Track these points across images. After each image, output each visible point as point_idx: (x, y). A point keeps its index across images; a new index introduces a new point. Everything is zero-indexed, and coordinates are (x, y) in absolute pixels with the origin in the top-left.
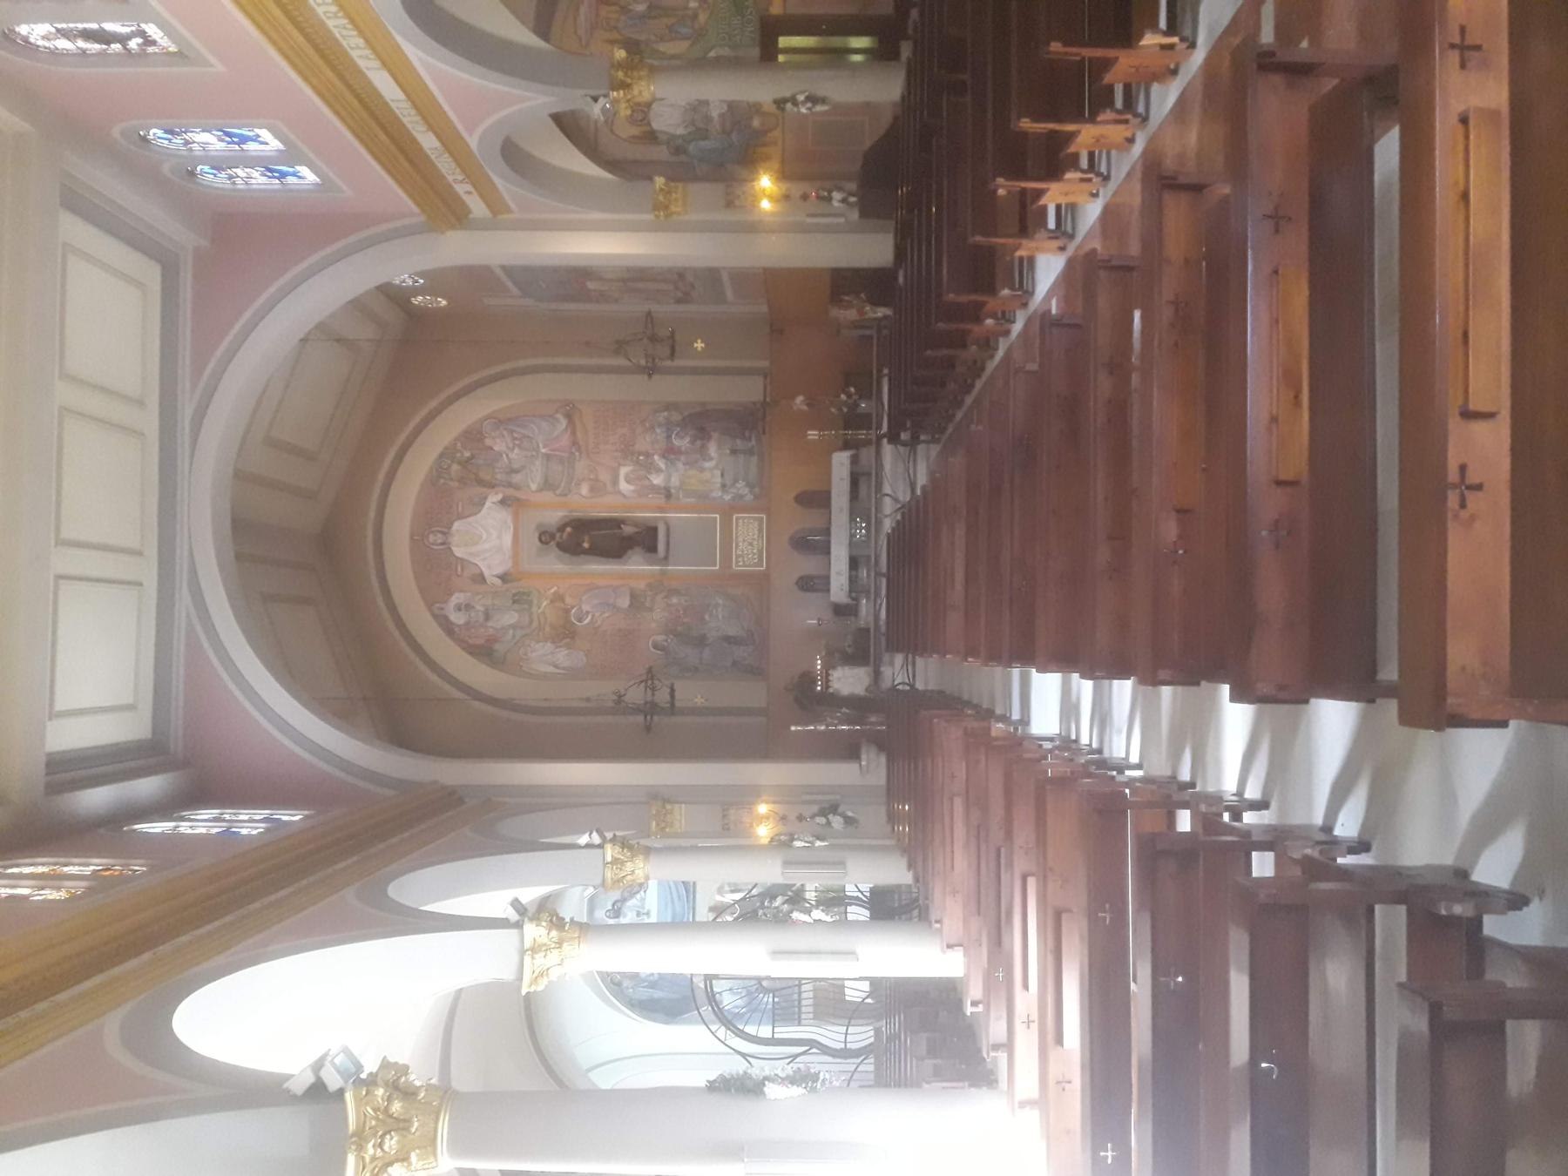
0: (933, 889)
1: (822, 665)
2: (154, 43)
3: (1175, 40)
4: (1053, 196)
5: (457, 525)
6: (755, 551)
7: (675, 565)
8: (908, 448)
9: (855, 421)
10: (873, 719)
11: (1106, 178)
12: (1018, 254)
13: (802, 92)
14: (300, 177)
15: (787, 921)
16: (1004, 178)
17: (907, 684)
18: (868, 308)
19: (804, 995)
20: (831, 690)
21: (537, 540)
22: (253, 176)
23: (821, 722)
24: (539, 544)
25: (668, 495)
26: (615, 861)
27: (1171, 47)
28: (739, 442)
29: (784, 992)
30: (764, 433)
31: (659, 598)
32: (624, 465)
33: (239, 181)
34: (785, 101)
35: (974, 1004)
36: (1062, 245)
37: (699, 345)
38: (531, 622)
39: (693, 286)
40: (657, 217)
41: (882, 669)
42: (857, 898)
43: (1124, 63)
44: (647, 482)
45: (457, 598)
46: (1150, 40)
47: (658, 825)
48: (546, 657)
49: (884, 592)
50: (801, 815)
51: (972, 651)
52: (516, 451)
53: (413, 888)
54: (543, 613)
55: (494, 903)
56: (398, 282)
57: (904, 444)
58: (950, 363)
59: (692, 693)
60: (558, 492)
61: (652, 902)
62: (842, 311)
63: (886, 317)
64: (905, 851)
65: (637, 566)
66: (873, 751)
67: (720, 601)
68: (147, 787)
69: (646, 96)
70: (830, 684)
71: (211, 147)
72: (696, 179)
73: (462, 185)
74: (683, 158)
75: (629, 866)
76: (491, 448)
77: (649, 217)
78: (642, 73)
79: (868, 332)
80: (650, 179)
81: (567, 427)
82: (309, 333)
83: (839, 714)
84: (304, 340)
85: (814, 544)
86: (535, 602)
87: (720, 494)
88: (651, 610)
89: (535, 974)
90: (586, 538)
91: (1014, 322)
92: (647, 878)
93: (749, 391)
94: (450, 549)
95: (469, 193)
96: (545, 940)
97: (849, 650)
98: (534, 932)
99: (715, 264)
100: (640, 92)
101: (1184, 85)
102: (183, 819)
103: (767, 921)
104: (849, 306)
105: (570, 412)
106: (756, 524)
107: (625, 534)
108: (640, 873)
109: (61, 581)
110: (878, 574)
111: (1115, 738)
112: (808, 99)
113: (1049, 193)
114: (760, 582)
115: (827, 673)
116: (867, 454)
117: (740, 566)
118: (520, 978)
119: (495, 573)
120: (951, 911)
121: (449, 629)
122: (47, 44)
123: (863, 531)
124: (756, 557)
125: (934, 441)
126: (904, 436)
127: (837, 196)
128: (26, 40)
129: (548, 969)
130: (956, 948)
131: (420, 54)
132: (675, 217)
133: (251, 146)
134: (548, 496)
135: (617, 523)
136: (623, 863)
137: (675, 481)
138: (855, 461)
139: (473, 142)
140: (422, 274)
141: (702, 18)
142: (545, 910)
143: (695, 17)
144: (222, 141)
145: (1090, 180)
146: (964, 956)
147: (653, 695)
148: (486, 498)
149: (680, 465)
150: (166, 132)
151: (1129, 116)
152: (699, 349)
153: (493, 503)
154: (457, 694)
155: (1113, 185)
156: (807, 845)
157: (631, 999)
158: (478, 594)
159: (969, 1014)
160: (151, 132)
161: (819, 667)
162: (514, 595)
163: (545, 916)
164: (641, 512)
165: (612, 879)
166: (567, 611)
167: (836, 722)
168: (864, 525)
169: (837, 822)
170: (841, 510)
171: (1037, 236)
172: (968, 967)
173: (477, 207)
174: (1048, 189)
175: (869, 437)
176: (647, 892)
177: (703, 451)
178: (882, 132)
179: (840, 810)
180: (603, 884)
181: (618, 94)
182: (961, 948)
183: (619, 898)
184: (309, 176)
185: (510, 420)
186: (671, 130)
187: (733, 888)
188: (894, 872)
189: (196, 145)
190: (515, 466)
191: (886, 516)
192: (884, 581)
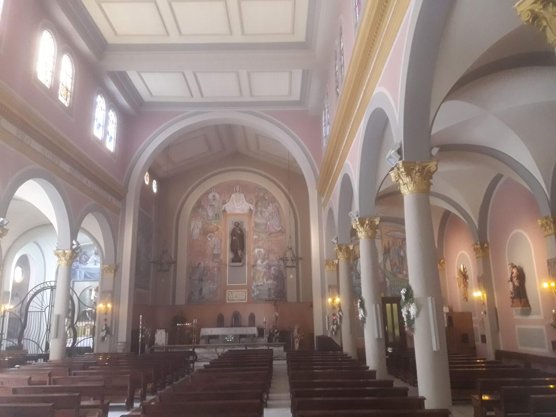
5: (242, 195)
13: (342, 314)
28: (273, 291)
31: (217, 264)
45: (217, 196)
47: (107, 267)
48: (197, 226)
52: (268, 214)
54: (212, 224)
60: (254, 228)
65: (229, 255)
67: (215, 286)
83: (148, 333)
87: (254, 285)
88: (213, 261)
90: (236, 238)
94: (234, 193)
106: (244, 298)
107: (238, 251)
134: (253, 224)
137: (259, 268)
143: (400, 273)
148: (251, 204)
149: (264, 270)
152: (291, 278)
153: (250, 207)
158: (219, 203)
161: (186, 324)
162: (218, 214)
166: (213, 232)
169: (103, 334)
179: (108, 335)
185: (279, 211)
190: (263, 214)
191: (216, 350)
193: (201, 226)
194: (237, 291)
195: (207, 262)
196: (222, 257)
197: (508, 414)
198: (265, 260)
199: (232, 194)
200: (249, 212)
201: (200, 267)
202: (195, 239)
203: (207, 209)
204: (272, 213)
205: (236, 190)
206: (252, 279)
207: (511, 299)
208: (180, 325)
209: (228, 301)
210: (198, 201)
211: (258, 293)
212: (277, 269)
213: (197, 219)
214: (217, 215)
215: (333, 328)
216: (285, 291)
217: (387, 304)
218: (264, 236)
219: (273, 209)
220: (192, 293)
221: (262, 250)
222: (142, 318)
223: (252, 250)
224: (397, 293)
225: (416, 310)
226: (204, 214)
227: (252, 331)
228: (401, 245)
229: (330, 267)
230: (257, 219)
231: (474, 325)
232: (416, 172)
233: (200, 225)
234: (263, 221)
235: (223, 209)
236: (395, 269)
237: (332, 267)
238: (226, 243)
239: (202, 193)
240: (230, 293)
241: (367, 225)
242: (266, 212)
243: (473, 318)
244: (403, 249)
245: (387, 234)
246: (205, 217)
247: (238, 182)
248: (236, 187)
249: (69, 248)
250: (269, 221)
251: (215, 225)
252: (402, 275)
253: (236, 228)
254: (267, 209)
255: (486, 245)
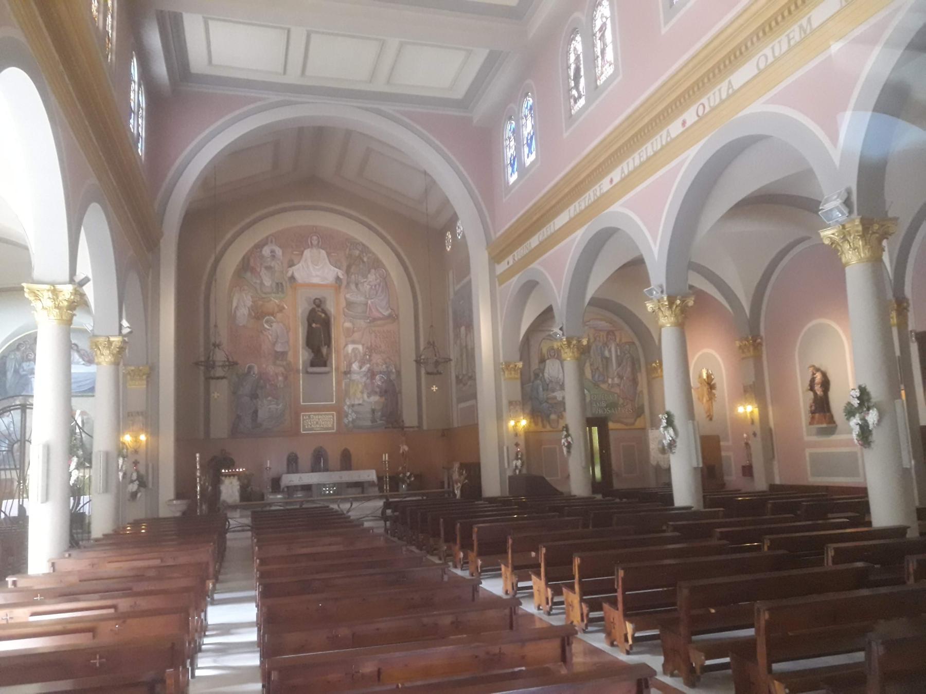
0: (95, 551)
1: (239, 472)
2: (575, 102)
3: (630, 642)
4: (537, 583)
5: (323, 252)
6: (313, 426)
8: (381, 516)
9: (395, 482)
10: (204, 507)
11: (549, 614)
13: (572, 440)
14: (511, 174)
15: (71, 454)
17: (229, 527)
18: (459, 484)
19: (8, 472)
20: (223, 478)
22: (511, 150)
24: (314, 298)
26: (110, 343)
27: (626, 640)
29: (11, 459)
30: (386, 428)
31: (282, 369)
32: (363, 348)
33: (508, 142)
34: (567, 431)
36: (508, 592)
37: (434, 388)
38: (265, 293)
39: (465, 385)
41: (238, 511)
42: (79, 503)
43: (615, 615)
44: (353, 360)
45: (279, 252)
46: (629, 627)
47: (132, 370)
48: (243, 304)
49: (288, 507)
51: (263, 562)
52: (368, 287)
53: (96, 217)
54: (271, 300)
55: (85, 268)
56: (458, 224)
57: (383, 513)
58: (436, 534)
59: (220, 393)
61: (79, 369)
62: (457, 469)
63: (455, 495)
65: (302, 356)
66: (184, 508)
67: (281, 406)
68: (160, 68)
69: (564, 356)
71: (524, 129)
72: (523, 384)
75: (106, 352)
77: (501, 360)
78: (576, 353)
79: (446, 486)
80: (521, 360)
82: (430, 176)
83: (207, 484)
84: (425, 173)
85: (319, 462)
87: (348, 403)
89: (37, 292)
90: (318, 326)
91: (462, 570)
92: (99, 364)
93: (409, 417)
94: (309, 248)
95: (508, 263)
96: (60, 298)
98: (67, 291)
99: (479, 396)
100: (566, 353)
101: (607, 651)
102: (139, 85)
104: (461, 474)
105: (393, 318)
106: (330, 426)
108: (101, 359)
109: (286, 31)
110: (302, 503)
111: (209, 659)
112: (569, 443)
114: (294, 432)
116: (375, 491)
117: (303, 417)
119: (294, 271)
120: (77, 564)
123: (328, 492)
124: (309, 427)
125: (386, 530)
126: (389, 512)
127: (519, 463)
128: (573, 39)
129: (40, 300)
130: (52, 568)
131: (580, 237)
132: (502, 373)
133: (526, 150)
134: (343, 304)
135: (328, 343)
136: (109, 348)
137: (355, 377)
138: (371, 484)
140: (464, 237)
141: (604, 386)
142: (78, 303)
143: (604, 382)
144: (528, 135)
145: (547, 603)
146: (43, 574)
148: (339, 269)
149: (364, 379)
150: (531, 107)
151: (585, 621)
153: (337, 273)
154: (219, 248)
155: (546, 618)
156: (120, 467)
157: (6, 357)
158: (282, 263)
159: (7, 579)
161: (237, 470)
162: (281, 284)
163: (78, 298)
164: (335, 357)
165: (98, 341)
166: (272, 314)
168: (331, 492)
169: (134, 487)
170: (341, 477)
171: (514, 577)
172: (36, 577)
173: (501, 268)
174: (541, 580)
175: (385, 491)
176: (83, 366)
178: (554, 485)
179: (142, 489)
180: (95, 336)
181: (565, 341)
182: (52, 571)
183: (80, 348)
184: (513, 178)
185: (386, 283)
186: (546, 371)
187: (85, 421)
188: (100, 526)
189: (525, 121)
190: (360, 286)
192: (298, 507)
193: (251, 303)
194: (318, 414)
196: (290, 354)
197: (627, 593)
199: (305, 249)
200: (336, 282)
202: (241, 325)
203: (261, 274)
204: (375, 286)
205: (311, 242)
207: (810, 414)
208: (227, 471)
210: (244, 258)
211: (354, 417)
212: (385, 378)
214: (280, 285)
215: (516, 464)
217: (596, 428)
218: (362, 323)
219: (376, 280)
220: (239, 417)
221: (360, 347)
222: (201, 458)
224: (600, 411)
226: (255, 283)
227: (368, 476)
228: (605, 339)
229: (511, 374)
230: (349, 294)
231: (723, 454)
232: (874, 233)
233: (249, 303)
234: (360, 299)
236: (597, 376)
239: (252, 245)
240: (307, 417)
241: (677, 306)
242: (365, 284)
243: (722, 443)
244: (608, 347)
246: (258, 287)
247: (314, 229)
248: (311, 238)
249: (117, 333)
251: (277, 301)
253: (317, 309)
254: (366, 277)
255: (759, 340)
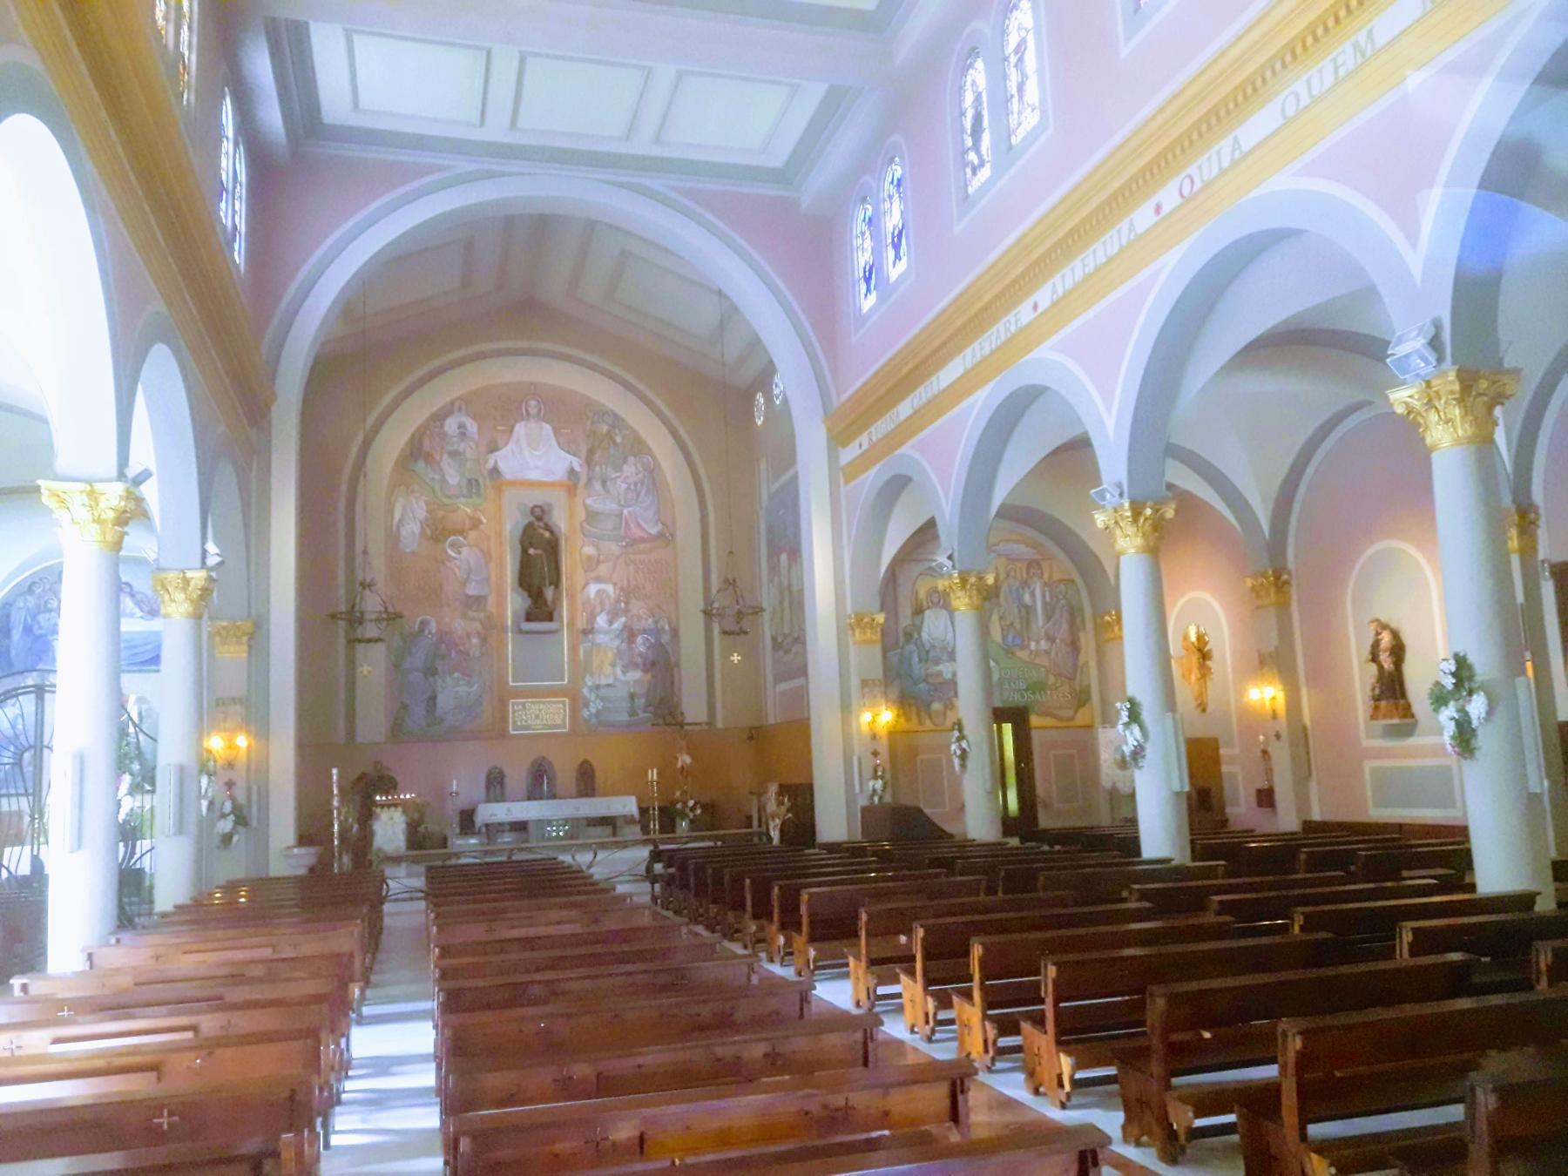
2: (974, 173)
3: (1067, 1088)
4: (909, 988)
5: (547, 428)
7: (513, 640)
8: (644, 873)
9: (668, 818)
11: (930, 1040)
12: (851, 961)
13: (969, 746)
14: (866, 295)
16: (925, 936)
21: (535, 503)
23: (342, 801)
24: (531, 505)
25: (586, 632)
26: (187, 581)
27: (1061, 1085)
28: (643, 701)
29: (19, 778)
30: (653, 725)
31: (477, 625)
32: (615, 589)
33: (860, 241)
34: (960, 730)
35: (24, 988)
38: (449, 497)
39: (787, 652)
40: (850, 617)
41: (404, 865)
42: (133, 853)
43: (1042, 1041)
44: (598, 610)
45: (472, 427)
46: (1066, 1062)
47: (224, 628)
48: (411, 515)
50: (234, 784)
51: (445, 952)
52: (624, 486)
54: (459, 508)
55: (143, 454)
56: (776, 380)
57: (649, 869)
58: (739, 906)
59: (373, 666)
60: (585, 525)
63: (770, 839)
64: (196, 901)
65: (513, 602)
67: (475, 688)
68: (272, 117)
69: (956, 603)
70: (386, 808)
72: (885, 651)
73: (867, 439)
74: (902, 640)
75: (180, 596)
76: (625, 462)
77: (849, 610)
78: (975, 599)
79: (755, 822)
80: (882, 609)
81: (650, 534)
83: (350, 820)
84: (720, 293)
85: (540, 782)
86: (470, 501)
87: (589, 683)
88: (464, 616)
89: (61, 494)
90: (539, 552)
93: (693, 709)
96: (102, 505)
97: (422, 829)
98: (113, 495)
99: (811, 672)
100: (959, 598)
101: (1027, 1104)
102: (236, 145)
103: (120, 748)
104: (781, 803)
105: (666, 538)
106: (559, 722)
107: (544, 589)
109: (485, 53)
111: (355, 1117)
112: (964, 751)
113: (911, 983)
114: (498, 732)
115: (400, 804)
116: (635, 832)
118: (57, 478)
121: (440, 417)
122: (968, 83)
125: (654, 899)
126: (658, 867)
127: (879, 784)
128: (971, 66)
129: (68, 508)
132: (850, 632)
134: (581, 514)
135: (556, 583)
136: (184, 589)
137: (601, 638)
138: (629, 820)
139: (903, 450)
140: (785, 401)
141: (1023, 655)
142: (133, 513)
143: (1023, 647)
145: (927, 1022)
147: (371, 621)
148: (575, 455)
149: (617, 642)
152: (732, 658)
155: (924, 1047)
157: (10, 605)
158: (477, 446)
160: (897, 167)
161: (402, 797)
162: (476, 481)
163: (132, 505)
165: (166, 578)
166: (461, 533)
167: (342, 818)
168: (561, 834)
169: (226, 825)
170: (577, 809)
171: (870, 977)
172: (61, 978)
173: (848, 454)
174: (916, 982)
177: (631, 665)
179: (241, 829)
180: (160, 569)
182: (87, 968)
184: (868, 303)
186: (925, 628)
190: (609, 483)
191: (573, 857)
192: (504, 858)
193: (425, 514)
195: (447, 620)
197: (1061, 1005)
198: (617, 615)
199: (516, 422)
200: (569, 478)
201: (427, 632)
202: (408, 550)
204: (635, 485)
205: (527, 411)
206: (580, 668)
208: (384, 798)
209: (565, 727)
211: (600, 707)
213: (412, 492)
214: (474, 482)
216: (675, 699)
218: (613, 548)
221: (610, 588)
222: (340, 776)
223: (579, 587)
225: (1487, 708)
226: (433, 479)
227: (624, 807)
228: (1025, 575)
231: (1225, 769)
232: (1479, 394)
233: (421, 513)
235: (490, 464)
236: (1010, 637)
237: (869, 631)
238: (501, 565)
240: (520, 707)
241: (1146, 519)
243: (1222, 751)
244: (1029, 588)
245: (995, 548)
246: (437, 486)
249: (198, 563)
250: (630, 506)
252: (1027, 652)
253: (536, 523)
254: (621, 470)
255: (1285, 577)
